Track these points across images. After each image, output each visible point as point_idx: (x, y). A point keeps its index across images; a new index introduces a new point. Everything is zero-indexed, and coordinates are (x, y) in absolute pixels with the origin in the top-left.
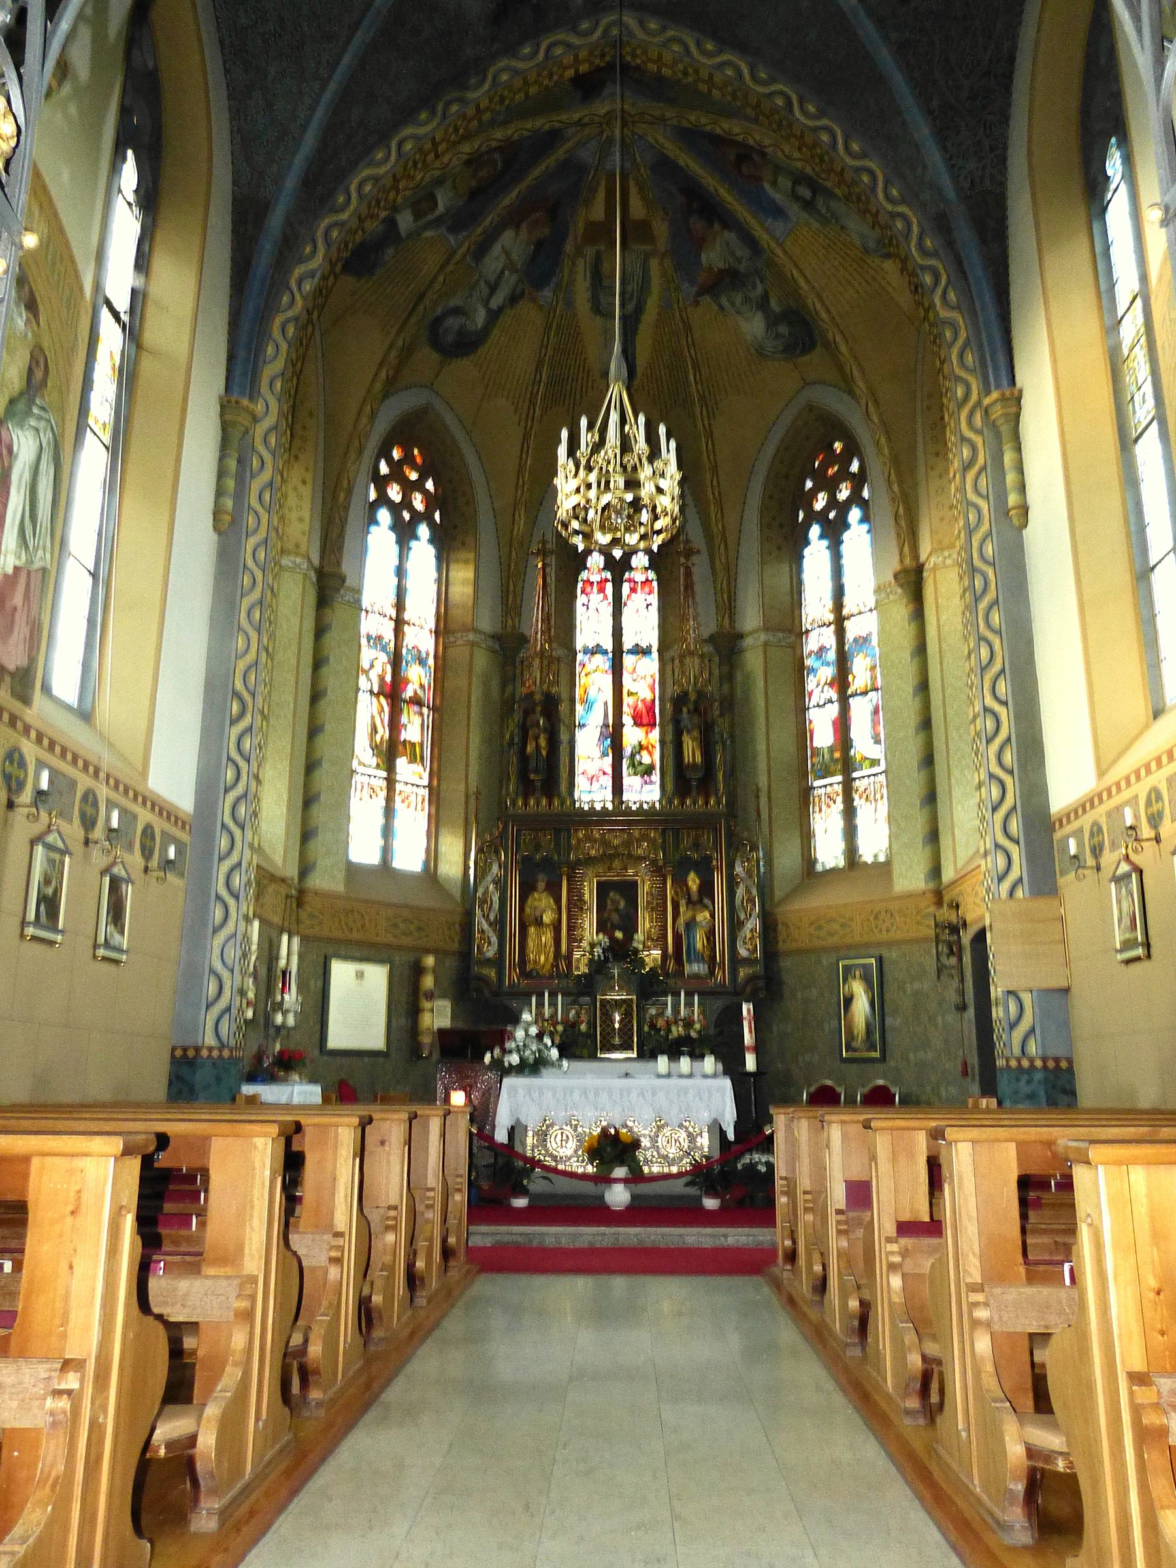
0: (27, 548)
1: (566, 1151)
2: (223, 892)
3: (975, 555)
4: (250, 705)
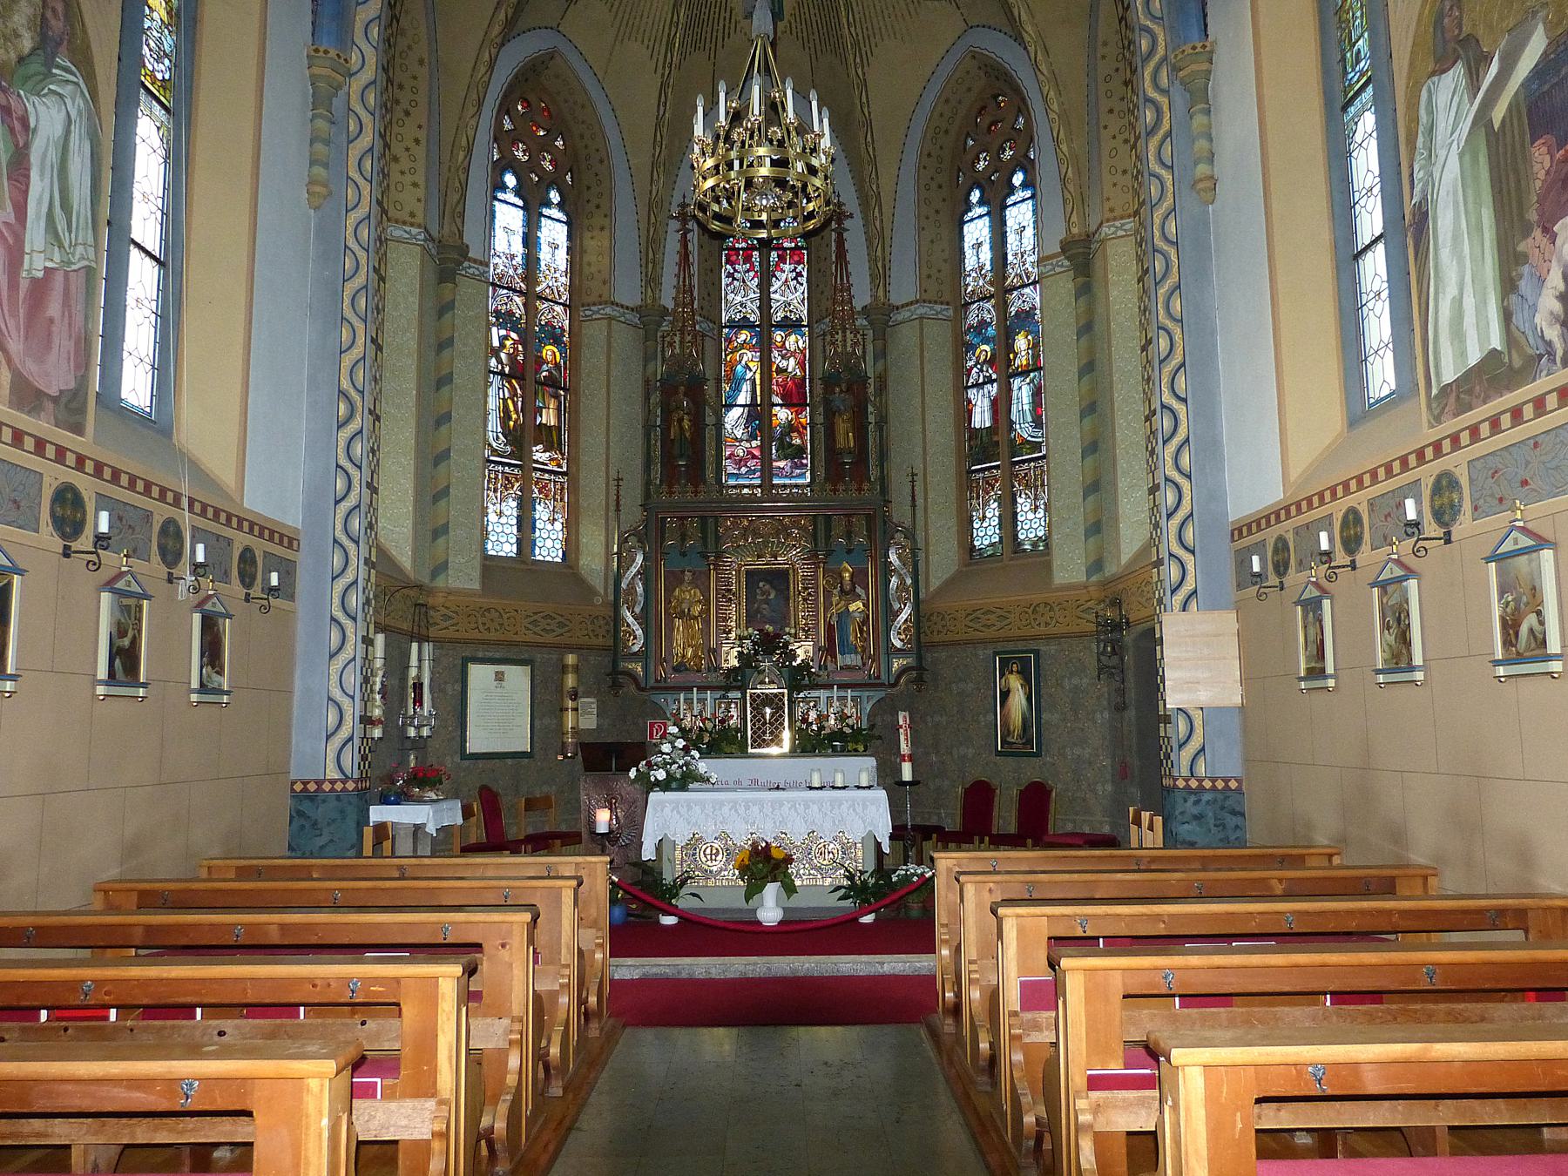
0: (61, 246)
1: (717, 885)
2: (339, 615)
3: (1174, 258)
4: (359, 404)
